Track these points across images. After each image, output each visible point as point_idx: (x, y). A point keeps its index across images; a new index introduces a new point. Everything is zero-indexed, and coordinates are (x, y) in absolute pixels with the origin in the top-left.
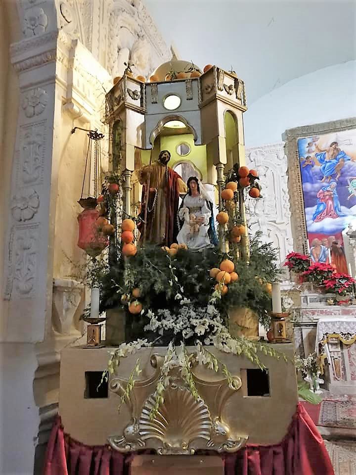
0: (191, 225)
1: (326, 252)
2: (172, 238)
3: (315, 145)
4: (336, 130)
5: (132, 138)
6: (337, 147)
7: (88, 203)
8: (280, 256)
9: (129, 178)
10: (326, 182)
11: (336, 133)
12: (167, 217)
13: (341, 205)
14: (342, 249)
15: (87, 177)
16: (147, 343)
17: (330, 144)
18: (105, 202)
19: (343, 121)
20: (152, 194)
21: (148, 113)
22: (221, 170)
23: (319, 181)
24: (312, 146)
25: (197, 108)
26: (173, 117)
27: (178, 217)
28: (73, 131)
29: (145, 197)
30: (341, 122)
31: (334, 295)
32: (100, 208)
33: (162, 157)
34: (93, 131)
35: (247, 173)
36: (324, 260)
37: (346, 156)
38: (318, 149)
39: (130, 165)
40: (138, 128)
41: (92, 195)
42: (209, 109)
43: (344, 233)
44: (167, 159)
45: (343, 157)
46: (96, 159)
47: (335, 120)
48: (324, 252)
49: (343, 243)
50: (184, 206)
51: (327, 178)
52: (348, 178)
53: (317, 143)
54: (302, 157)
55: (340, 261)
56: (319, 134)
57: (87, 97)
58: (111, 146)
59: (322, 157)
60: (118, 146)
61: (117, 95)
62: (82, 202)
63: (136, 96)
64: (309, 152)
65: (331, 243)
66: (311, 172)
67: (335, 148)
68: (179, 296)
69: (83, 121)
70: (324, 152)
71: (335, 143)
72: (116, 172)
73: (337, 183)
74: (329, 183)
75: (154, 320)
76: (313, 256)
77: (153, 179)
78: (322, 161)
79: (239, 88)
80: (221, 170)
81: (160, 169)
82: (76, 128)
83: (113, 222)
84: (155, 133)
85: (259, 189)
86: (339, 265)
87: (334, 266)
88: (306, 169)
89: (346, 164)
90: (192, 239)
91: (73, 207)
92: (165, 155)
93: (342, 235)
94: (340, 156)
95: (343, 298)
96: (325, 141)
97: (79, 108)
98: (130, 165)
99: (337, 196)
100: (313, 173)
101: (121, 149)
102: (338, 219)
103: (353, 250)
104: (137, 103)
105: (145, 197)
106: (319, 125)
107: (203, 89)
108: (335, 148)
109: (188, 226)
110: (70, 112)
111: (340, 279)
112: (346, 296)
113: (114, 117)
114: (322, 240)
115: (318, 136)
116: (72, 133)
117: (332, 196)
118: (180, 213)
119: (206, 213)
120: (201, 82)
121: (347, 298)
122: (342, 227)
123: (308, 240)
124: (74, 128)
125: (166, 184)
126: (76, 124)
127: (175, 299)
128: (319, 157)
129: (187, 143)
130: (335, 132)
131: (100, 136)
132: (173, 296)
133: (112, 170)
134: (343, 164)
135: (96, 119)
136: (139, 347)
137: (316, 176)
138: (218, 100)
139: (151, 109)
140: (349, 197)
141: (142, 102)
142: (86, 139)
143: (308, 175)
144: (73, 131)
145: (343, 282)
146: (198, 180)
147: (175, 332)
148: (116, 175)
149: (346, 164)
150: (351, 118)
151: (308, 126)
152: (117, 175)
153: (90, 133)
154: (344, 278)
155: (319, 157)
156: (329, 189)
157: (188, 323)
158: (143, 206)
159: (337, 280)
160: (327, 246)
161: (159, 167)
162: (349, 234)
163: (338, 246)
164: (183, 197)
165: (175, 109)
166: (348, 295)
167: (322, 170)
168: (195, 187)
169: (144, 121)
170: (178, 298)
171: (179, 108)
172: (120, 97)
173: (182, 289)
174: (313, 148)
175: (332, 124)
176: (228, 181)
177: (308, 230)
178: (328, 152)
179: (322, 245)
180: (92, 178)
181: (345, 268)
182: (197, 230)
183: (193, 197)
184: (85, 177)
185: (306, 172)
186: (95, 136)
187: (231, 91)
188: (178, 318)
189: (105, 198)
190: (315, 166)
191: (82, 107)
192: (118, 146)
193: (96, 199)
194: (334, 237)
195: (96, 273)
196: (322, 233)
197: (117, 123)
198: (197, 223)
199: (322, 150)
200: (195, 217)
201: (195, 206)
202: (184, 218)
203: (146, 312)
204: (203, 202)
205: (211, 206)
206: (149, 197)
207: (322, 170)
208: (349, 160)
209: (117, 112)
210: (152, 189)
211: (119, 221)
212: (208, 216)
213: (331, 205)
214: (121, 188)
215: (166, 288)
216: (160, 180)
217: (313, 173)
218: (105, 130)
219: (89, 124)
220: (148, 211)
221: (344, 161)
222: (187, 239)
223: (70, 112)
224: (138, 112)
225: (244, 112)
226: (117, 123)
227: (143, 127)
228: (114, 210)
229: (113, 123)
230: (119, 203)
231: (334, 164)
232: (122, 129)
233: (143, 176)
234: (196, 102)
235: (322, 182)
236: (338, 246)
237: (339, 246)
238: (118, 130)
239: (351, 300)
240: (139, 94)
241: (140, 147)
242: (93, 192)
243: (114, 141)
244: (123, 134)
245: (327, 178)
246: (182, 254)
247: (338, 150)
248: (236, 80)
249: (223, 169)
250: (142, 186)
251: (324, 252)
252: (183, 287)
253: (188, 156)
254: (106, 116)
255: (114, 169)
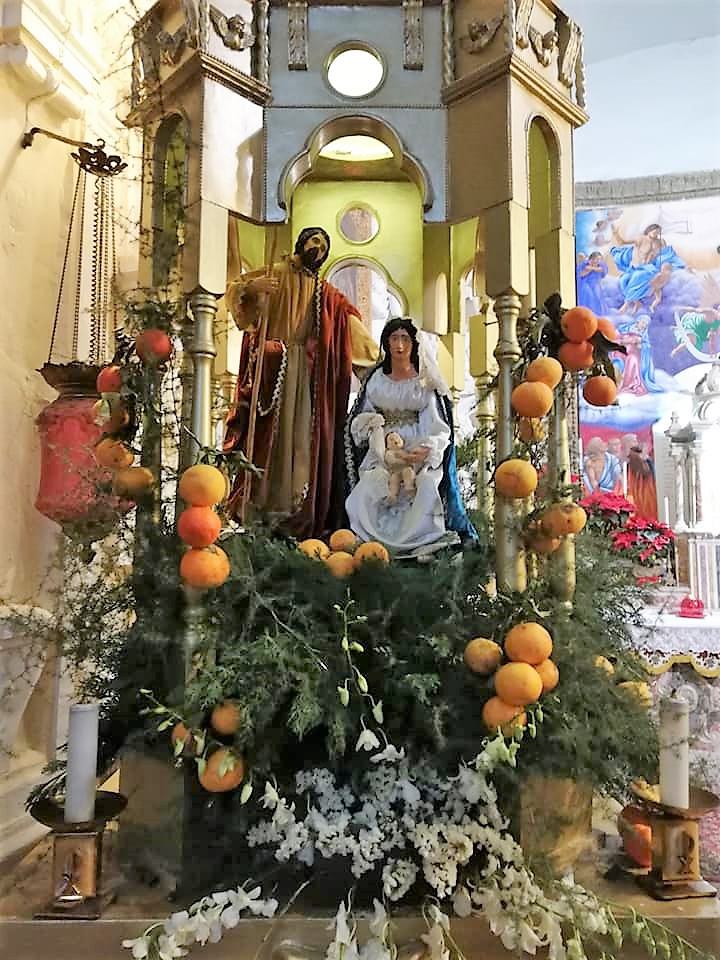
0: (392, 468)
1: (617, 468)
2: (329, 516)
3: (613, 227)
4: (659, 197)
5: (222, 181)
6: (659, 237)
7: (74, 380)
8: (187, 186)
9: (210, 317)
10: (629, 314)
11: (658, 204)
12: (314, 434)
13: (656, 367)
14: (650, 463)
15: (70, 281)
16: (261, 902)
17: (643, 228)
18: (125, 392)
19: (678, 179)
20: (273, 361)
21: (274, 103)
22: (511, 314)
23: (614, 310)
24: (605, 228)
25: (435, 98)
26: (361, 123)
27: (346, 436)
28: (26, 142)
29: (249, 369)
30: (673, 179)
31: (628, 563)
32: (107, 415)
33: (307, 248)
34: (90, 146)
35: (590, 329)
36: (611, 484)
37: (675, 258)
38: (619, 239)
39: (213, 275)
40: (241, 149)
41: (83, 356)
42: (484, 104)
43: (658, 430)
44: (321, 255)
45: (671, 261)
46: (100, 240)
47: (659, 173)
48: (612, 467)
49: (653, 450)
50: (368, 404)
51: (632, 304)
52: (676, 309)
53: (616, 223)
54: (583, 254)
55: (644, 487)
56: (621, 203)
57: (74, 31)
58: (149, 200)
59: (625, 256)
60: (173, 203)
61: (172, 28)
62: (49, 371)
63: (237, 38)
64: (597, 242)
65: (629, 450)
66: (597, 289)
67: (655, 239)
68: (368, 739)
69: (61, 111)
70: (629, 246)
71: (657, 227)
72: (165, 291)
73: (652, 318)
74: (635, 316)
75: (283, 815)
76: (588, 476)
77: (279, 302)
78: (623, 265)
79: (568, 49)
80: (511, 314)
81: (700, 594)
82: (35, 130)
83: (150, 458)
84: (298, 170)
85: (614, 380)
86: (640, 495)
87: (630, 499)
88: (587, 282)
89: (675, 276)
90: (392, 511)
91: (25, 383)
92: (317, 241)
93: (651, 433)
94: (663, 258)
95: (648, 573)
96: (634, 220)
97: (45, 66)
98: (213, 275)
99: (649, 346)
100: (602, 291)
101: (181, 215)
102: (647, 398)
103: (676, 468)
104: (241, 61)
105: (249, 369)
106: (625, 181)
107: (458, 35)
108: (655, 239)
109: (381, 471)
110: (16, 76)
111: (645, 530)
112: (655, 567)
113: (161, 103)
114: (610, 441)
115: (620, 208)
116: (24, 147)
117: (640, 346)
118: (357, 426)
119: (433, 434)
120: (452, 12)
121: (656, 571)
122: (656, 416)
123: (581, 440)
124: (28, 131)
125: (314, 328)
126: (37, 117)
127: (358, 748)
128: (618, 255)
129: (369, 207)
130: (658, 200)
131: (114, 164)
132: (352, 737)
133: (148, 282)
134: (669, 277)
135: (102, 108)
136: (232, 918)
137: (607, 299)
138: (512, 78)
139: (286, 87)
140: (674, 352)
141: (255, 62)
142: (70, 169)
143: (591, 294)
144: (26, 142)
145: (651, 537)
146: (416, 331)
147: (357, 870)
148: (163, 300)
149: (675, 276)
150: (695, 173)
151: (601, 183)
152: (168, 302)
153: (81, 150)
154: (654, 529)
155: (618, 255)
156: (633, 329)
157: (397, 835)
158: (245, 397)
159: (639, 533)
160: (618, 454)
161: (297, 278)
162: (671, 433)
163: (641, 456)
164: (361, 375)
165: (366, 97)
166: (658, 565)
167: (622, 287)
168: (406, 351)
169: (261, 126)
170: (368, 748)
171: (380, 95)
172: (182, 33)
173: (378, 712)
174: (608, 234)
175: (652, 183)
176: (530, 353)
177: (581, 419)
178: (639, 245)
179: (609, 452)
180: (86, 301)
181: (652, 505)
182: (408, 486)
183: (396, 380)
184: (63, 288)
185: (587, 287)
186: (97, 161)
187: (547, 52)
188: (370, 862)
189: (125, 379)
190: (607, 276)
191: (57, 63)
192: (173, 203)
193: (97, 369)
194: (635, 436)
195: (84, 636)
196: (607, 420)
197: (171, 124)
198: (408, 462)
199: (627, 240)
200: (401, 444)
201: (402, 409)
202: (367, 441)
203: (259, 791)
204: (427, 398)
205: (447, 409)
206: (261, 369)
207: (622, 287)
208: (682, 267)
209: (172, 87)
210: (271, 345)
211: (170, 459)
212: (441, 443)
213: (634, 367)
214: (178, 345)
215: (327, 713)
216: (296, 319)
217: (602, 291)
218: (129, 146)
219: (78, 122)
220: (258, 413)
221: (670, 269)
222: (379, 511)
223: (16, 76)
224: (244, 94)
225: (577, 126)
226: (171, 124)
227: (257, 146)
228: (152, 414)
229: (157, 124)
230: (170, 394)
231: (649, 274)
232: (187, 148)
233: (247, 303)
234: (431, 83)
235: (618, 315)
236: (641, 456)
237: (644, 456)
238: (172, 147)
239: (662, 576)
240: (248, 30)
241: (247, 213)
242: (90, 346)
243: (159, 185)
244: (192, 166)
245: (632, 304)
246: (367, 579)
247: (660, 243)
248: (561, 18)
249: (516, 311)
250: (242, 332)
251: (612, 467)
252: (380, 703)
253: (369, 246)
254: (135, 96)
255: (157, 282)
